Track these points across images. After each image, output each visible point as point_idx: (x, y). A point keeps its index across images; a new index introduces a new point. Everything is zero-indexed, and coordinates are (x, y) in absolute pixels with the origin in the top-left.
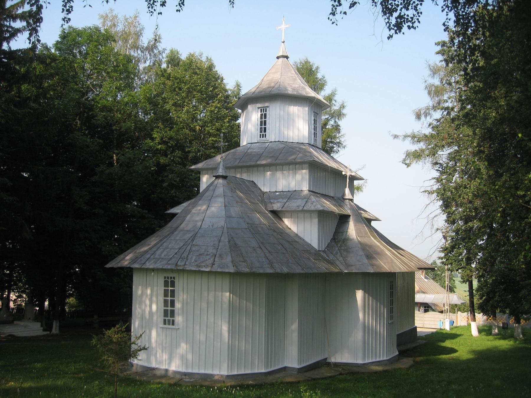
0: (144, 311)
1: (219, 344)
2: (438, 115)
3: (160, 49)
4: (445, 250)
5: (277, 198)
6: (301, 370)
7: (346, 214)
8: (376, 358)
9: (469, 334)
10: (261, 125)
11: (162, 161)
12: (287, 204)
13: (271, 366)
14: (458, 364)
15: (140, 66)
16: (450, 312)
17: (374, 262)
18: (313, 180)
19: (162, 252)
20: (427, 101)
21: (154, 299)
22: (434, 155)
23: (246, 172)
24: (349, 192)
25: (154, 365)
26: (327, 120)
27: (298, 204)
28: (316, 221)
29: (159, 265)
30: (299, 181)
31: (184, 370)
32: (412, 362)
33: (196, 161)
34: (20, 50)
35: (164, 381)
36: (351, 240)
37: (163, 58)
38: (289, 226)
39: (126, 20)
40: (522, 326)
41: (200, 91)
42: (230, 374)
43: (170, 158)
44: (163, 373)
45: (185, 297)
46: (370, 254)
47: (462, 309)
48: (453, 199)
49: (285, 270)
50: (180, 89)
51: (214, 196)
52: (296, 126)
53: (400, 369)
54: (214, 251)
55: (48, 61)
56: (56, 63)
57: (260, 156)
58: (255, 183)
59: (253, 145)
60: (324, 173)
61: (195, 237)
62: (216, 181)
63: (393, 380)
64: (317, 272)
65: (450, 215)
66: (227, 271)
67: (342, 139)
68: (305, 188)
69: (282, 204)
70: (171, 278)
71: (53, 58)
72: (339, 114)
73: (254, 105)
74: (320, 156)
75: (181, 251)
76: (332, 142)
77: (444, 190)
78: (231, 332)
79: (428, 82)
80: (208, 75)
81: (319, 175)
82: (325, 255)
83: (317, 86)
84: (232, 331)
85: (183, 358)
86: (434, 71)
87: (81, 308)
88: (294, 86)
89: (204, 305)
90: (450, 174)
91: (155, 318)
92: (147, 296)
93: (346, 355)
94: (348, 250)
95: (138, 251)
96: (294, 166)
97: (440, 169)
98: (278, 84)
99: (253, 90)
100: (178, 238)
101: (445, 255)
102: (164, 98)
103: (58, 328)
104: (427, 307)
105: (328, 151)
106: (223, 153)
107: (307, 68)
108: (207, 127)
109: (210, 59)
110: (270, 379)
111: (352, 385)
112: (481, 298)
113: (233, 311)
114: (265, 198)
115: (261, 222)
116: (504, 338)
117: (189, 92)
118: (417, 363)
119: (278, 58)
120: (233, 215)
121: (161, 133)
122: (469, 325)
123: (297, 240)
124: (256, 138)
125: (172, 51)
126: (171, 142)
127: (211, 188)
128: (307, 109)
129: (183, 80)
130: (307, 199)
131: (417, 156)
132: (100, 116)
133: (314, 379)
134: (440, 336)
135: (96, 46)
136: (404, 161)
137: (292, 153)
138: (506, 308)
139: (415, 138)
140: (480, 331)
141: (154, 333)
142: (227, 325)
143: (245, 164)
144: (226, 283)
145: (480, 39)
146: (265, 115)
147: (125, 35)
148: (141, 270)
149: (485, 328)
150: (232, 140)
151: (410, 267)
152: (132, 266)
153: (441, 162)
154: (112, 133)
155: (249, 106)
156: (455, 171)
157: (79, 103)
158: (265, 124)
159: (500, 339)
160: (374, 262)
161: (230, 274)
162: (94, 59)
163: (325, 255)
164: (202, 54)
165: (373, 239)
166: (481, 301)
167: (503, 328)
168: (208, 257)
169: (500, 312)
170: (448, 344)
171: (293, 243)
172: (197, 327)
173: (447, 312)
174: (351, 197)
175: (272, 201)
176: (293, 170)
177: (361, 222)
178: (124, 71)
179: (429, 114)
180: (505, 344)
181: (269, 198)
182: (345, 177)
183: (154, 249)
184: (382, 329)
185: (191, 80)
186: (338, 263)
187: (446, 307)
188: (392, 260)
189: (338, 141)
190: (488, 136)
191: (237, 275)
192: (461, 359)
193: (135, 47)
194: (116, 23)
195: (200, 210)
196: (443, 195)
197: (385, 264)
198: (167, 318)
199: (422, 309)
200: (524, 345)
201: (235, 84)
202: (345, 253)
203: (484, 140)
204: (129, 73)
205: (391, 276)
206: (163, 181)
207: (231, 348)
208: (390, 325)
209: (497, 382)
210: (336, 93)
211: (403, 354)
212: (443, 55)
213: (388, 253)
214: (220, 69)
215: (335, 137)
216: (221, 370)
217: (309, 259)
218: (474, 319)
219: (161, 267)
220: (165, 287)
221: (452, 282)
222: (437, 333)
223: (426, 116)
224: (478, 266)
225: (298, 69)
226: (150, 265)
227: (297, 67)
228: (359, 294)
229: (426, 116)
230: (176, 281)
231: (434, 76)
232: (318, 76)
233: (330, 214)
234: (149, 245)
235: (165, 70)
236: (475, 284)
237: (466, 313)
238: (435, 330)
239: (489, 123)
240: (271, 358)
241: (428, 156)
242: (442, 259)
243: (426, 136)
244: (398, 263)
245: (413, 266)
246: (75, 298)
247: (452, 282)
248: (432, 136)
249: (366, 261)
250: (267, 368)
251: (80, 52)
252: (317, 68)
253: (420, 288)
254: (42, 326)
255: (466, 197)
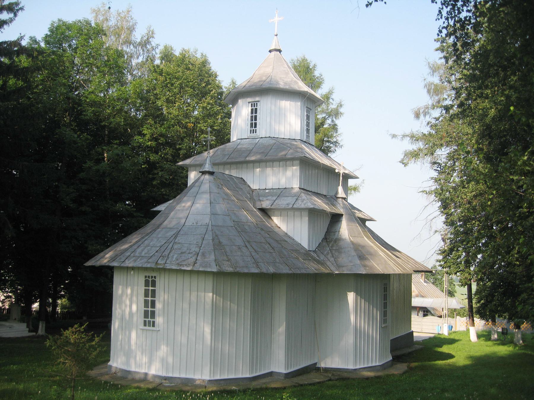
0: (124, 311)
1: (201, 346)
2: (437, 113)
3: (153, 44)
4: (444, 253)
5: (266, 195)
6: (288, 376)
7: (339, 213)
8: (364, 364)
9: (468, 339)
10: (252, 120)
11: (152, 158)
12: (276, 201)
13: (256, 370)
14: (455, 370)
15: (133, 61)
16: (449, 316)
17: (367, 263)
18: (303, 177)
19: (143, 250)
20: (426, 100)
21: (135, 299)
22: (432, 154)
23: (234, 169)
24: (342, 190)
25: (133, 369)
26: (325, 119)
27: (287, 202)
28: (306, 219)
29: (138, 264)
30: (289, 178)
31: (164, 374)
32: (406, 368)
33: (187, 156)
34: (5, 42)
35: (142, 385)
36: (343, 240)
37: (156, 53)
38: (279, 225)
39: (119, 14)
40: (522, 332)
41: (193, 87)
42: (212, 379)
43: (161, 156)
44: (142, 376)
45: (166, 297)
46: (362, 254)
47: (461, 314)
48: (452, 199)
49: (272, 270)
50: (172, 85)
51: (200, 192)
52: (287, 121)
53: (393, 375)
54: (197, 250)
55: (35, 54)
56: (43, 57)
57: (250, 152)
58: (244, 180)
59: (243, 140)
60: (317, 171)
61: (178, 234)
62: (203, 177)
63: (385, 387)
64: (305, 272)
65: (448, 215)
66: (209, 270)
67: (339, 139)
68: (296, 185)
69: (271, 202)
70: (152, 277)
71: (41, 52)
72: (336, 113)
73: (244, 100)
74: (313, 153)
75: (163, 249)
76: (328, 141)
77: (442, 190)
78: (213, 334)
79: (428, 81)
80: (201, 71)
81: (310, 172)
82: (315, 255)
83: (315, 84)
84: (214, 333)
85: (163, 361)
86: (434, 69)
87: (73, 310)
88: (285, 80)
89: (186, 306)
90: (448, 174)
91: (135, 319)
92: (127, 296)
93: (337, 359)
94: (339, 250)
95: (118, 249)
96: (284, 163)
97: (439, 169)
98: (270, 77)
99: (244, 84)
100: (160, 236)
101: (444, 258)
102: (156, 94)
103: (44, 328)
104: (426, 312)
105: (326, 151)
106: (211, 149)
107: (304, 66)
108: (199, 123)
109: (205, 56)
110: (254, 384)
111: (340, 392)
112: (479, 302)
113: (216, 312)
114: (254, 195)
115: (248, 219)
116: (503, 344)
117: (181, 88)
118: (411, 369)
119: (270, 51)
120: (219, 212)
121: (151, 129)
122: (468, 330)
123: (286, 239)
124: (246, 134)
125: (166, 47)
126: (162, 139)
127: (197, 184)
128: (299, 104)
129: (175, 76)
130: (297, 197)
131: (415, 155)
132: (89, 112)
133: (302, 385)
134: (438, 341)
135: (85, 40)
136: (402, 162)
137: (284, 149)
138: (504, 313)
139: (414, 138)
140: (479, 336)
141: (134, 335)
142: (210, 328)
143: (233, 160)
144: (209, 282)
145: (471, 10)
146: (256, 109)
147: (117, 30)
148: (121, 268)
149: (485, 333)
150: (222, 136)
151: (404, 269)
152: (110, 265)
153: (440, 162)
154: (101, 129)
155: (240, 101)
156: (454, 170)
157: (68, 98)
158: (256, 119)
159: (499, 344)
160: (367, 263)
161: (213, 273)
162: (84, 53)
163: (315, 255)
164: (197, 50)
165: (366, 239)
166: (478, 305)
167: (503, 333)
168: (190, 255)
169: (499, 317)
170: (445, 349)
171: (281, 243)
172: (178, 329)
173: (448, 319)
174: (344, 196)
175: (261, 198)
176: (283, 166)
177: (354, 221)
178: (115, 66)
179: (428, 113)
180: (504, 350)
181: (259, 195)
182: (338, 174)
183: (135, 247)
184: (375, 333)
185: (183, 75)
186: (328, 263)
187: (444, 312)
188: (385, 261)
189: (335, 140)
190: (487, 133)
191: (220, 275)
192: (457, 365)
193: (128, 42)
194: (108, 18)
195: (184, 207)
196: (440, 194)
197: (378, 265)
198: (147, 320)
199: (421, 313)
200: (523, 351)
201: (230, 81)
202: (337, 254)
203: (483, 137)
204: (120, 67)
205: (385, 278)
206: (154, 179)
207: (213, 351)
208: (384, 329)
209: (493, 391)
210: (334, 91)
211: (397, 359)
212: (443, 51)
213: (381, 253)
214: (214, 66)
215: (332, 136)
216: (203, 374)
217: (298, 259)
218: (473, 324)
219: (140, 266)
220: (145, 286)
221: (452, 286)
222: (434, 338)
223: (425, 115)
224: (477, 269)
225: (295, 68)
226: (129, 263)
227: (294, 64)
228: (351, 296)
229: (425, 115)
230: (157, 280)
231: (433, 75)
232: (315, 74)
233: (322, 212)
234: (130, 242)
235: (158, 66)
236: (474, 287)
237: (465, 318)
238: (432, 335)
239: (488, 120)
240: (257, 362)
241: (426, 155)
242: (440, 262)
243: (425, 135)
244: (392, 264)
245: (408, 269)
246: (68, 300)
247: (452, 286)
248: (430, 135)
249: (358, 262)
250: (252, 373)
251: (70, 46)
252: (315, 66)
253: (419, 292)
254: (28, 327)
255: (464, 197)
